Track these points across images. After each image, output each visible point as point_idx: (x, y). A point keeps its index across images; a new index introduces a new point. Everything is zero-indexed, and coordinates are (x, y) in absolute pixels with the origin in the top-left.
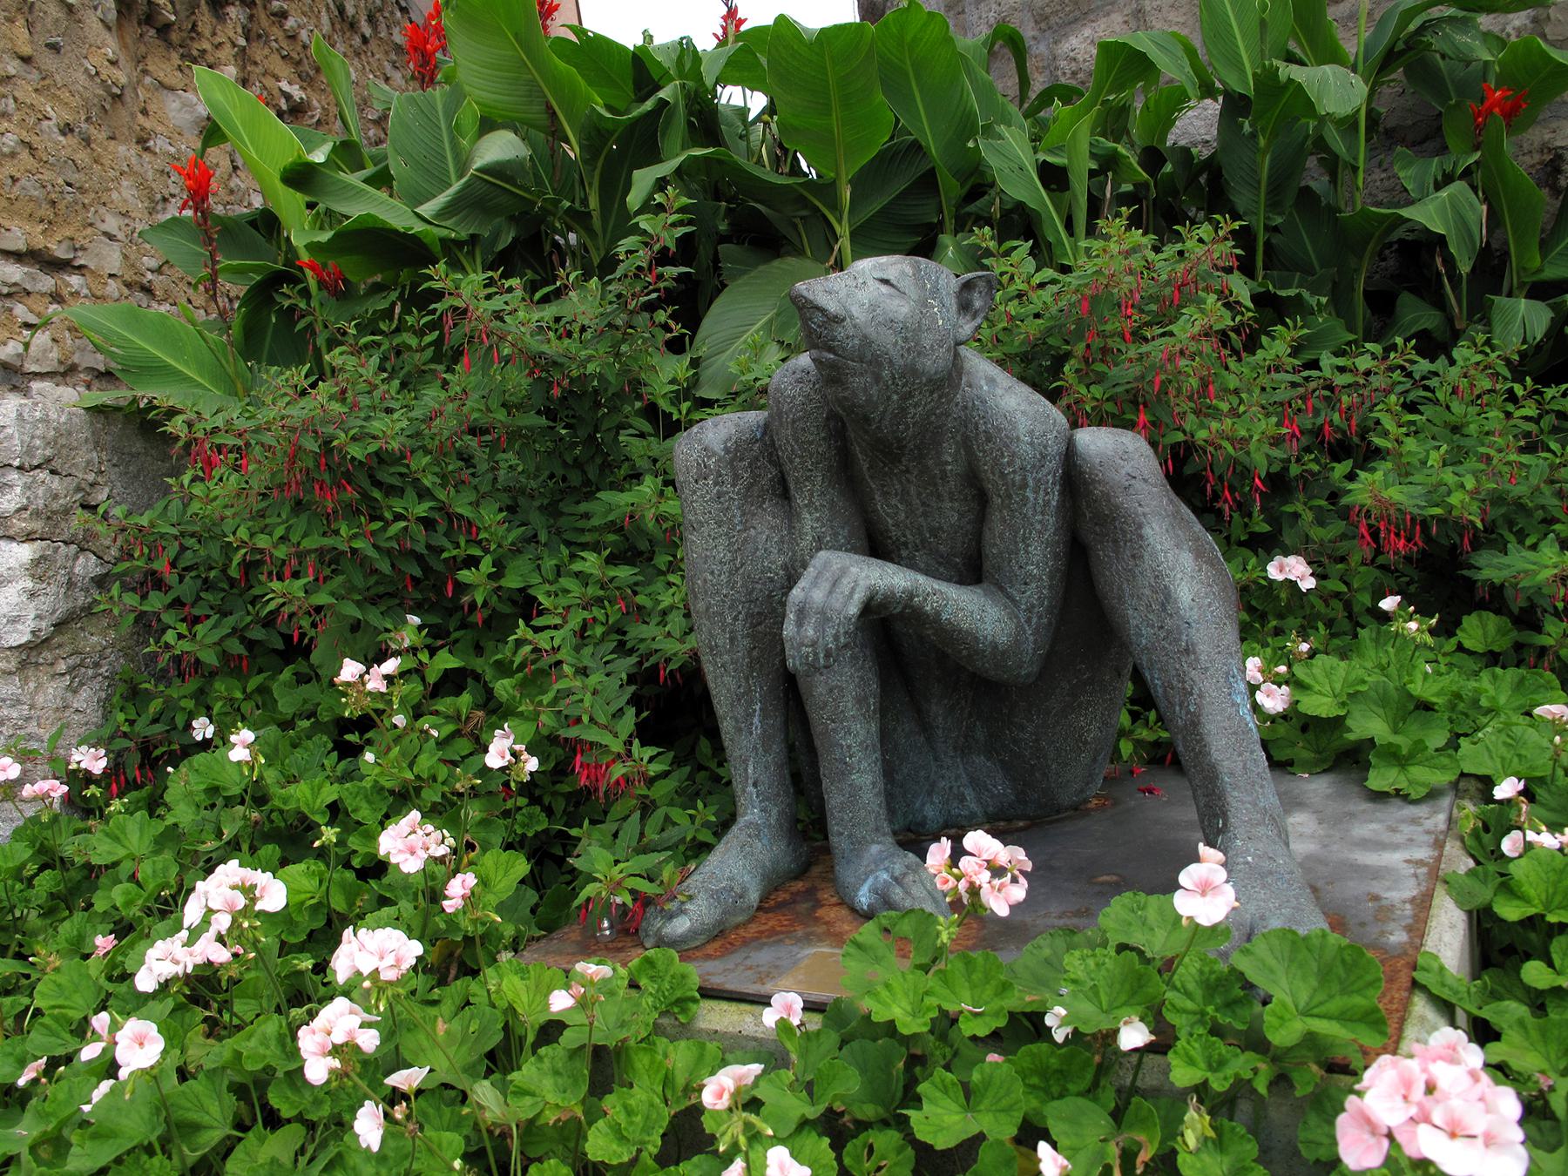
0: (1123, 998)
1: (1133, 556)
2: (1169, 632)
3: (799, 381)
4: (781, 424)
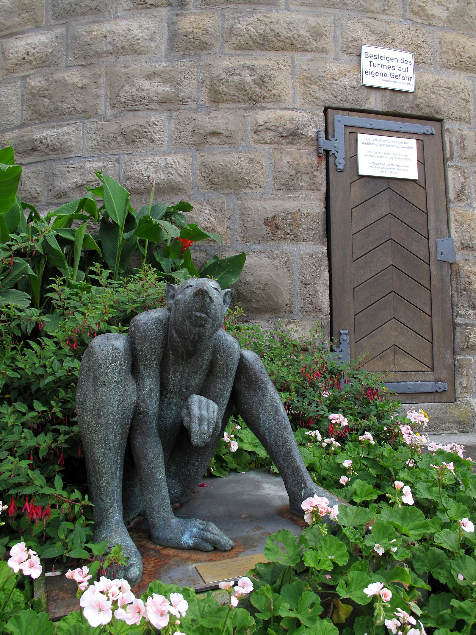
0: (381, 537)
1: (263, 395)
2: (278, 421)
3: (155, 323)
4: (145, 341)
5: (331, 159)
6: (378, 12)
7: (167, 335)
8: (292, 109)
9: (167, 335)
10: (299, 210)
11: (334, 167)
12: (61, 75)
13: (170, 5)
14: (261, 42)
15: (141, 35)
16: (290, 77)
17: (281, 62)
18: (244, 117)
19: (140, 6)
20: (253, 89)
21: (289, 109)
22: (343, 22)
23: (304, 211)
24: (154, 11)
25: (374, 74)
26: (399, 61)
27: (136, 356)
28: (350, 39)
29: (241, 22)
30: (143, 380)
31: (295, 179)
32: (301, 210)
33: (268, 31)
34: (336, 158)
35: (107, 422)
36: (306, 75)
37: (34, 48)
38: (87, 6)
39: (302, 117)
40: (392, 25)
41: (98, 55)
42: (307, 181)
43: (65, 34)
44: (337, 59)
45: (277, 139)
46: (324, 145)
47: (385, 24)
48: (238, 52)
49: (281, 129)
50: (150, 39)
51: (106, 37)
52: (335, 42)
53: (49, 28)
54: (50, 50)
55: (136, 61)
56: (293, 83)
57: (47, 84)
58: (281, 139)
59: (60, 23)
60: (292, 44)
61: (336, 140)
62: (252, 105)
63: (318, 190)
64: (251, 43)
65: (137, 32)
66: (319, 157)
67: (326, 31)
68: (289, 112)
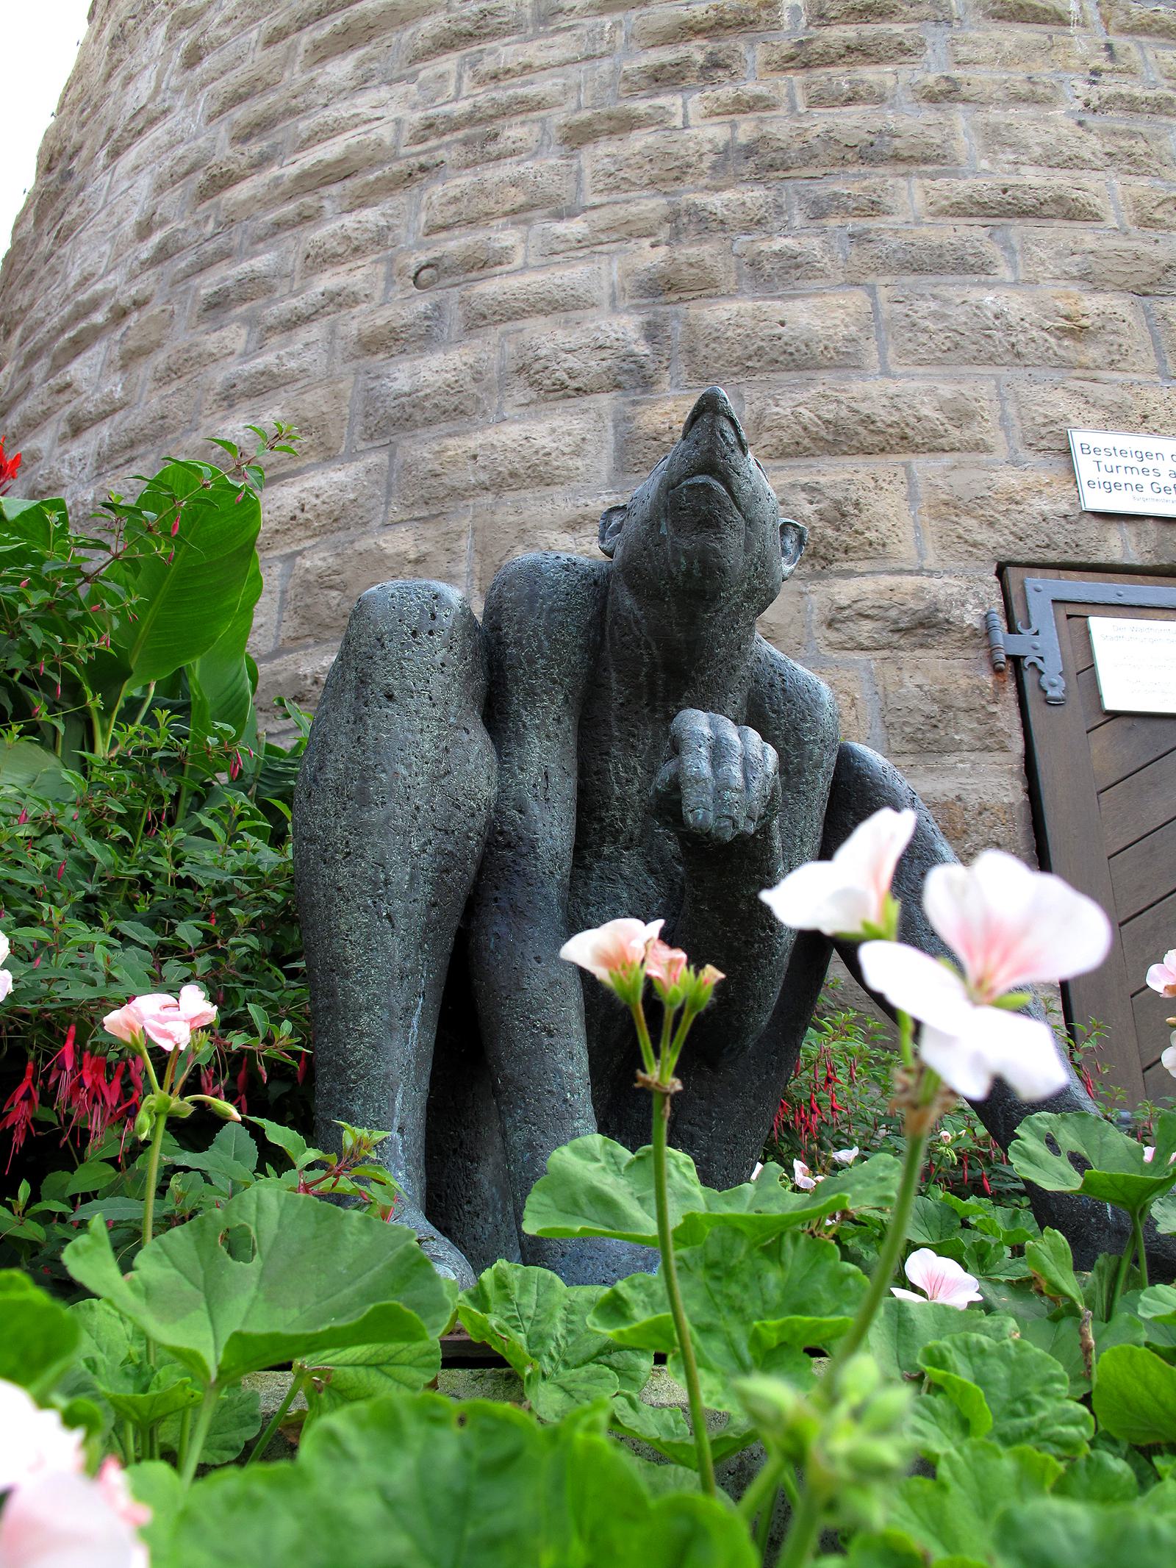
4: (532, 610)
5: (1029, 677)
6: (1098, 367)
7: (602, 613)
8: (919, 572)
9: (602, 613)
10: (959, 798)
11: (1040, 694)
12: (372, 541)
13: (618, 386)
14: (830, 438)
15: (555, 445)
16: (905, 505)
17: (881, 475)
18: (801, 594)
19: (552, 395)
20: (818, 531)
21: (910, 572)
22: (1018, 389)
23: (972, 800)
24: (585, 402)
25: (1111, 488)
26: (1168, 457)
27: (500, 667)
28: (1040, 420)
29: (781, 403)
30: (520, 740)
31: (940, 725)
32: (964, 796)
33: (844, 413)
34: (1041, 673)
35: (388, 818)
36: (944, 497)
37: (317, 496)
38: (436, 406)
39: (943, 587)
40: (1136, 389)
41: (456, 494)
42: (972, 730)
43: (387, 463)
44: (1015, 463)
45: (886, 637)
46: (1006, 643)
47: (1119, 390)
48: (778, 463)
49: (893, 613)
50: (573, 453)
51: (475, 457)
52: (1006, 429)
53: (352, 456)
54: (352, 496)
55: (543, 498)
56: (914, 517)
57: (339, 561)
58: (896, 636)
59: (377, 444)
60: (904, 438)
61: (1037, 633)
62: (818, 568)
63: (1003, 749)
64: (806, 442)
65: (546, 442)
66: (998, 672)
67: (982, 407)
68: (910, 579)
